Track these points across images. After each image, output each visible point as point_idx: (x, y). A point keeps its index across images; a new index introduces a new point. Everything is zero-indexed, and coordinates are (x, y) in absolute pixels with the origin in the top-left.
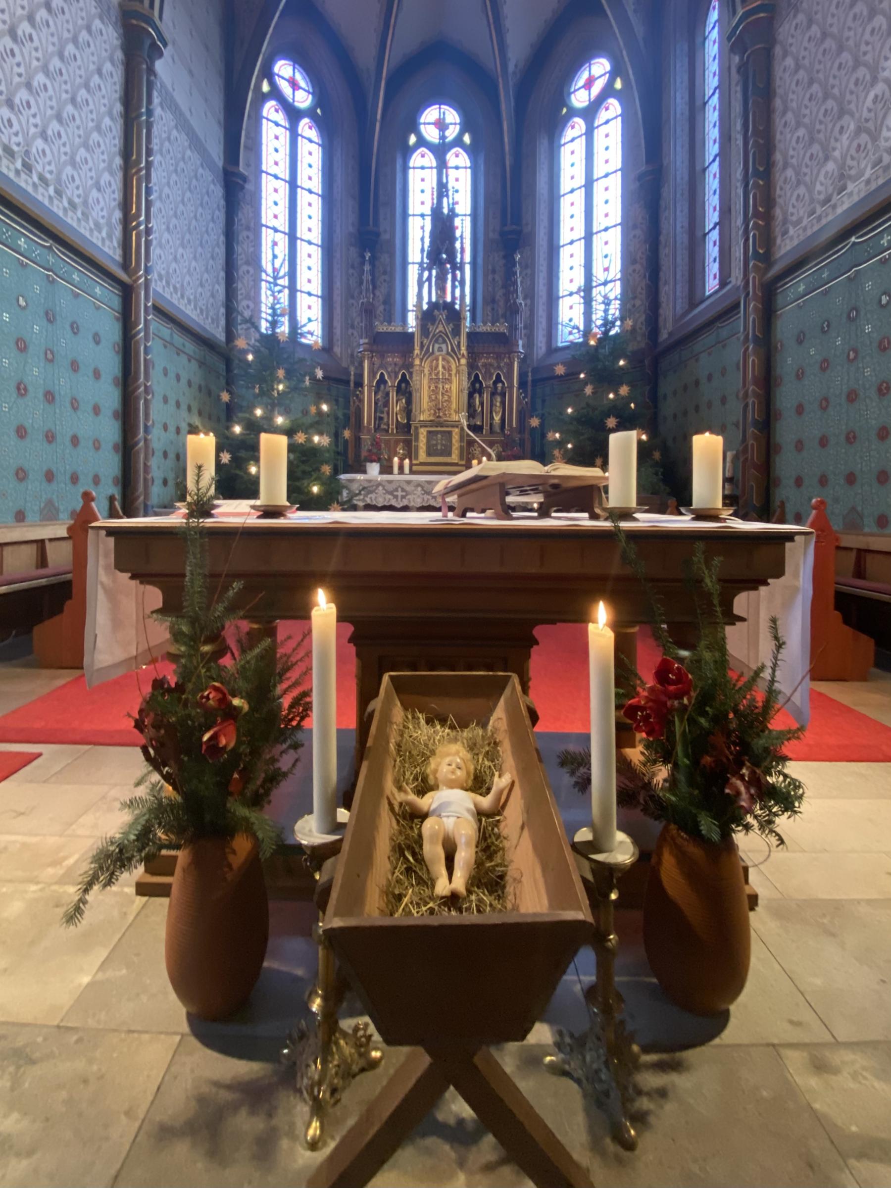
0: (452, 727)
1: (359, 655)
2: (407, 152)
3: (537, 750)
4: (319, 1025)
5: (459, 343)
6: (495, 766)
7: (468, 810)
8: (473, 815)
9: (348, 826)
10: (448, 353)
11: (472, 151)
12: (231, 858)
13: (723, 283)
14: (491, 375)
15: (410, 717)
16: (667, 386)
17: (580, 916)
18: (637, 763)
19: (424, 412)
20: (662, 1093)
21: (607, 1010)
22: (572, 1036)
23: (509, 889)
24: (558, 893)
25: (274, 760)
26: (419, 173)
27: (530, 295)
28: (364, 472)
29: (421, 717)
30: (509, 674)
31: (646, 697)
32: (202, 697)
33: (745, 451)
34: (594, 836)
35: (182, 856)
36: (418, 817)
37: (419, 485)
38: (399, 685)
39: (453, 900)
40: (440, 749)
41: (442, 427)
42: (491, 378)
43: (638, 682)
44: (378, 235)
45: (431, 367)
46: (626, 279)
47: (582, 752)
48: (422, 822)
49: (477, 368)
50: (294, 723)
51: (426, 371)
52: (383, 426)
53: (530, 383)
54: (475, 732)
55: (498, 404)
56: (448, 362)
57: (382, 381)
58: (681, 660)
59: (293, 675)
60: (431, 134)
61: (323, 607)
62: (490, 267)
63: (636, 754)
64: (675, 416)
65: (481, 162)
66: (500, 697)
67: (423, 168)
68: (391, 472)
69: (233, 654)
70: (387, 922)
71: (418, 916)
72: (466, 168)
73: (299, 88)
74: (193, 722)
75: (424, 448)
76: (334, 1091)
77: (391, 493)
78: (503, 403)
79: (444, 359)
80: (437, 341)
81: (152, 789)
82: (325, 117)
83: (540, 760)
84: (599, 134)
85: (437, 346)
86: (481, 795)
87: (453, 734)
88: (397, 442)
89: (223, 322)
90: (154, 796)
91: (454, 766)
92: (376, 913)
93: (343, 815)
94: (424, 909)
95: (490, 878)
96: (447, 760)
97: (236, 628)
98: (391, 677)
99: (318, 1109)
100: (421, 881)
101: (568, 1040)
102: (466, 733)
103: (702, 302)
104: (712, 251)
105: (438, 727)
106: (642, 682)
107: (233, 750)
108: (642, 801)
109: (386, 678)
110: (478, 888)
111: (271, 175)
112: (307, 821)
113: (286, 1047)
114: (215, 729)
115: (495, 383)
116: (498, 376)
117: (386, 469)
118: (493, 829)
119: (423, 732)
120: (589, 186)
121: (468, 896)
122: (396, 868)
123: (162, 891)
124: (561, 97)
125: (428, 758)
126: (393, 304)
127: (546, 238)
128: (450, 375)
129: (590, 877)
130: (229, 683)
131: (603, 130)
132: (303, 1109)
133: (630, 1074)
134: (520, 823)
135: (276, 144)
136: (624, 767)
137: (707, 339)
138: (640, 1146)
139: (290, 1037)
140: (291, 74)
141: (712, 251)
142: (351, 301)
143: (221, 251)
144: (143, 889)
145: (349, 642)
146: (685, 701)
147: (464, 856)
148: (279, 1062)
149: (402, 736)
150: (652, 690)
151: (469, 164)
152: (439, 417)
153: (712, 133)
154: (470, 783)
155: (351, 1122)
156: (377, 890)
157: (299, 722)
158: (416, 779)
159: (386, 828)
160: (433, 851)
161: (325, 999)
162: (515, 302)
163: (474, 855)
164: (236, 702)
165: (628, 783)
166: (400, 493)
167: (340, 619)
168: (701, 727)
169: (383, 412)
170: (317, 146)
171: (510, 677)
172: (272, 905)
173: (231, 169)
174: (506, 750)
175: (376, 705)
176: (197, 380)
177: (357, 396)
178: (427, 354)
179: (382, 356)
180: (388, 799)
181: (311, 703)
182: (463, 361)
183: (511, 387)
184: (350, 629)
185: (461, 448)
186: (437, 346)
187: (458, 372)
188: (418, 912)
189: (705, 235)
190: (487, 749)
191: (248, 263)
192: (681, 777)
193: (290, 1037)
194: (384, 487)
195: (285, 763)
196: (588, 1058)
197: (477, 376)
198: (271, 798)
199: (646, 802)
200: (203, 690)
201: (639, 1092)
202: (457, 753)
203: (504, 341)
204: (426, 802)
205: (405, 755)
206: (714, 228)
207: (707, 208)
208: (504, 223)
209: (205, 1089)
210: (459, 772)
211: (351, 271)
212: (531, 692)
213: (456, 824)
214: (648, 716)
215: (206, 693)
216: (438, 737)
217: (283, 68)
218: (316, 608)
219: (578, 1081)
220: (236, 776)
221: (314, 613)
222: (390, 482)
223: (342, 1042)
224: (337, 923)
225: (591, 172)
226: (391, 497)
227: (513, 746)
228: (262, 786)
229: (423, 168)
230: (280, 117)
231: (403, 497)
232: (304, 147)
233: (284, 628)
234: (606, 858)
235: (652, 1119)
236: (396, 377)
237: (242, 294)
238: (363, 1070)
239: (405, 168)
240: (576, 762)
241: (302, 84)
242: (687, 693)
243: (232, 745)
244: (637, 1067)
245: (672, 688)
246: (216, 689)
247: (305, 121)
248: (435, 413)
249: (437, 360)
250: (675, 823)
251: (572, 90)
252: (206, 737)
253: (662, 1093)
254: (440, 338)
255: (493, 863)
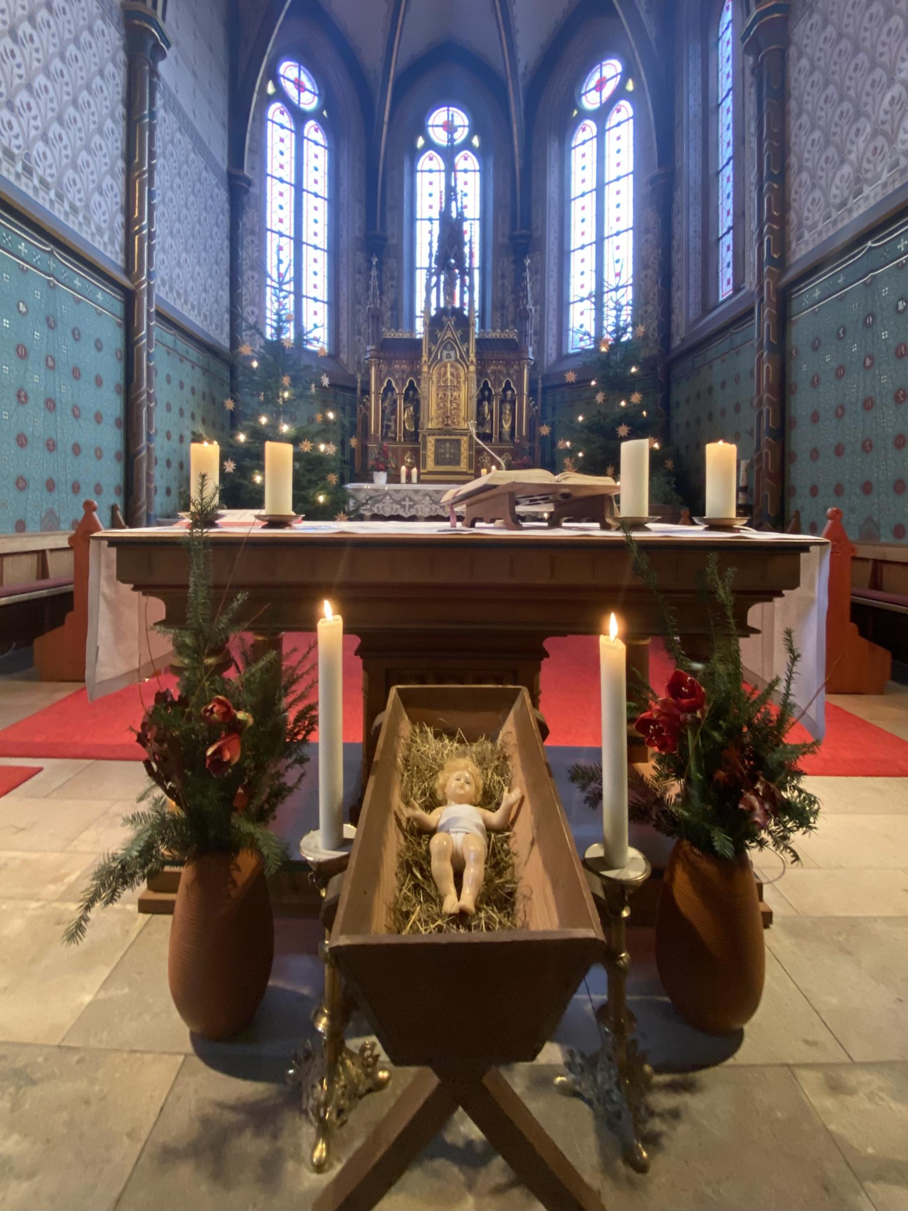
0: (461, 741)
1: (365, 668)
2: (415, 155)
3: (547, 765)
4: (325, 1045)
5: (468, 349)
6: (504, 781)
7: (477, 826)
8: (482, 831)
9: (355, 842)
10: (457, 360)
11: (481, 154)
12: (235, 874)
13: (737, 289)
14: (501, 382)
15: (418, 731)
16: (679, 394)
17: (591, 934)
18: (649, 777)
19: (432, 420)
20: (675, 1114)
21: (618, 1030)
22: (583, 1056)
23: (519, 906)
24: (569, 910)
25: (279, 775)
26: (427, 177)
27: (540, 300)
28: (371, 481)
29: (430, 731)
30: (519, 687)
31: (659, 710)
32: (206, 711)
33: (759, 460)
34: (606, 853)
35: (185, 872)
36: (426, 833)
37: (427, 494)
38: (406, 699)
39: (461, 918)
40: (448, 764)
41: (450, 435)
42: (500, 385)
43: (651, 695)
44: (385, 239)
45: (439, 374)
46: (638, 284)
47: (593, 767)
48: (430, 838)
49: (487, 375)
50: (300, 737)
51: (435, 379)
52: (390, 435)
53: (540, 391)
54: (484, 746)
55: (508, 412)
56: (457, 369)
57: (389, 388)
58: (694, 673)
59: (299, 688)
60: (439, 137)
61: (330, 619)
62: (499, 273)
63: (648, 769)
64: (688, 424)
65: (490, 165)
66: (510, 710)
67: (431, 171)
68: (398, 481)
69: (237, 667)
70: (394, 939)
71: (426, 933)
72: (475, 171)
73: (305, 90)
74: (197, 736)
75: (433, 456)
76: (340, 1112)
77: (398, 503)
78: (513, 411)
79: (452, 366)
80: (445, 348)
81: (155, 804)
82: (332, 120)
83: (551, 775)
84: (610, 137)
85: (445, 353)
86: (490, 810)
87: (461, 748)
88: (405, 451)
89: (227, 328)
90: (157, 812)
91: (462, 781)
92: (383, 931)
93: (349, 831)
94: (432, 926)
95: (499, 895)
96: (456, 775)
97: (240, 640)
98: (398, 690)
99: (324, 1130)
100: (429, 899)
101: (578, 1060)
102: (475, 748)
103: (716, 307)
104: (726, 256)
105: (447, 741)
106: (654, 695)
107: (238, 764)
108: (654, 817)
109: (393, 691)
110: (488, 905)
111: (276, 178)
112: (313, 837)
113: (292, 1067)
114: (219, 743)
115: (504, 390)
116: (508, 383)
117: (394, 478)
118: (502, 845)
119: (431, 746)
120: (600, 189)
121: (477, 913)
122: (403, 885)
123: (165, 908)
124: (571, 99)
125: (437, 772)
126: (400, 310)
127: (556, 243)
128: (459, 382)
129: (601, 894)
130: (233, 696)
131: (614, 133)
132: (309, 1130)
133: (642, 1095)
134: (530, 839)
135: (282, 146)
136: (636, 782)
137: (721, 346)
138: (652, 1168)
139: (296, 1057)
140: (297, 75)
141: (726, 256)
142: (358, 307)
143: (225, 256)
144: (145, 906)
145: (356, 654)
146: (699, 715)
147: (473, 873)
148: (285, 1083)
149: (409, 750)
150: (664, 703)
151: (478, 168)
152: (447, 425)
153: (726, 136)
154: (479, 798)
155: (358, 1143)
156: (385, 907)
157: (305, 736)
158: (424, 794)
159: (394, 844)
160: (441, 868)
161: (331, 1018)
162: (525, 308)
163: (483, 872)
164: (241, 715)
165: (640, 798)
166: (407, 503)
167: (347, 631)
168: (715, 742)
169: (390, 420)
170: (323, 149)
171: (519, 690)
172: (277, 923)
173: (235, 172)
174: (516, 765)
175: (383, 718)
176: (201, 387)
177: (364, 404)
178: (435, 361)
179: (390, 363)
180: (396, 814)
181: (317, 716)
182: (472, 368)
183: (521, 394)
184: (356, 641)
185: (470, 456)
186: (445, 353)
187: (467, 379)
188: (426, 930)
189: (719, 239)
190: (497, 763)
191: (252, 268)
192: (694, 792)
193: (296, 1057)
194: (391, 496)
195: (290, 777)
196: (599, 1079)
197: (486, 383)
198: (277, 813)
199: (658, 817)
200: (207, 704)
201: (652, 1114)
202: (466, 768)
203: (514, 348)
204: (434, 818)
205: (413, 770)
206: (728, 232)
207: (720, 212)
208: (513, 227)
209: (209, 1110)
210: (467, 787)
211: (358, 276)
212: (541, 705)
213: (464, 840)
214: (660, 730)
215: (210, 707)
216: (447, 752)
217: (289, 70)
218: (322, 620)
219: (589, 1102)
220: (240, 791)
221: (320, 625)
222: (397, 491)
223: (348, 1062)
224: (344, 941)
225: (602, 175)
226: (398, 506)
227: (523, 760)
228: (267, 801)
229: (431, 171)
230: (286, 120)
231: (411, 507)
232: (310, 150)
233: (289, 640)
234: (618, 875)
235: (664, 1141)
236: (404, 384)
237: (246, 300)
238: (370, 1091)
239: (413, 172)
240: (587, 777)
241: (308, 85)
242: (700, 706)
243: (236, 759)
244: (650, 1088)
245: (685, 701)
246: (220, 702)
247: (311, 124)
248: (444, 420)
249: (446, 367)
250: (688, 839)
251: (583, 92)
252: (210, 752)
253: (675, 1114)
254: (448, 345)
255: (502, 880)
